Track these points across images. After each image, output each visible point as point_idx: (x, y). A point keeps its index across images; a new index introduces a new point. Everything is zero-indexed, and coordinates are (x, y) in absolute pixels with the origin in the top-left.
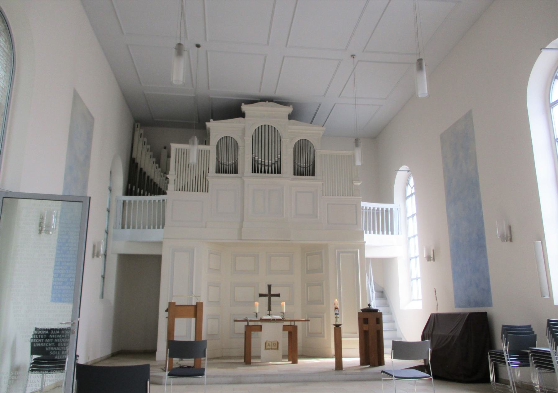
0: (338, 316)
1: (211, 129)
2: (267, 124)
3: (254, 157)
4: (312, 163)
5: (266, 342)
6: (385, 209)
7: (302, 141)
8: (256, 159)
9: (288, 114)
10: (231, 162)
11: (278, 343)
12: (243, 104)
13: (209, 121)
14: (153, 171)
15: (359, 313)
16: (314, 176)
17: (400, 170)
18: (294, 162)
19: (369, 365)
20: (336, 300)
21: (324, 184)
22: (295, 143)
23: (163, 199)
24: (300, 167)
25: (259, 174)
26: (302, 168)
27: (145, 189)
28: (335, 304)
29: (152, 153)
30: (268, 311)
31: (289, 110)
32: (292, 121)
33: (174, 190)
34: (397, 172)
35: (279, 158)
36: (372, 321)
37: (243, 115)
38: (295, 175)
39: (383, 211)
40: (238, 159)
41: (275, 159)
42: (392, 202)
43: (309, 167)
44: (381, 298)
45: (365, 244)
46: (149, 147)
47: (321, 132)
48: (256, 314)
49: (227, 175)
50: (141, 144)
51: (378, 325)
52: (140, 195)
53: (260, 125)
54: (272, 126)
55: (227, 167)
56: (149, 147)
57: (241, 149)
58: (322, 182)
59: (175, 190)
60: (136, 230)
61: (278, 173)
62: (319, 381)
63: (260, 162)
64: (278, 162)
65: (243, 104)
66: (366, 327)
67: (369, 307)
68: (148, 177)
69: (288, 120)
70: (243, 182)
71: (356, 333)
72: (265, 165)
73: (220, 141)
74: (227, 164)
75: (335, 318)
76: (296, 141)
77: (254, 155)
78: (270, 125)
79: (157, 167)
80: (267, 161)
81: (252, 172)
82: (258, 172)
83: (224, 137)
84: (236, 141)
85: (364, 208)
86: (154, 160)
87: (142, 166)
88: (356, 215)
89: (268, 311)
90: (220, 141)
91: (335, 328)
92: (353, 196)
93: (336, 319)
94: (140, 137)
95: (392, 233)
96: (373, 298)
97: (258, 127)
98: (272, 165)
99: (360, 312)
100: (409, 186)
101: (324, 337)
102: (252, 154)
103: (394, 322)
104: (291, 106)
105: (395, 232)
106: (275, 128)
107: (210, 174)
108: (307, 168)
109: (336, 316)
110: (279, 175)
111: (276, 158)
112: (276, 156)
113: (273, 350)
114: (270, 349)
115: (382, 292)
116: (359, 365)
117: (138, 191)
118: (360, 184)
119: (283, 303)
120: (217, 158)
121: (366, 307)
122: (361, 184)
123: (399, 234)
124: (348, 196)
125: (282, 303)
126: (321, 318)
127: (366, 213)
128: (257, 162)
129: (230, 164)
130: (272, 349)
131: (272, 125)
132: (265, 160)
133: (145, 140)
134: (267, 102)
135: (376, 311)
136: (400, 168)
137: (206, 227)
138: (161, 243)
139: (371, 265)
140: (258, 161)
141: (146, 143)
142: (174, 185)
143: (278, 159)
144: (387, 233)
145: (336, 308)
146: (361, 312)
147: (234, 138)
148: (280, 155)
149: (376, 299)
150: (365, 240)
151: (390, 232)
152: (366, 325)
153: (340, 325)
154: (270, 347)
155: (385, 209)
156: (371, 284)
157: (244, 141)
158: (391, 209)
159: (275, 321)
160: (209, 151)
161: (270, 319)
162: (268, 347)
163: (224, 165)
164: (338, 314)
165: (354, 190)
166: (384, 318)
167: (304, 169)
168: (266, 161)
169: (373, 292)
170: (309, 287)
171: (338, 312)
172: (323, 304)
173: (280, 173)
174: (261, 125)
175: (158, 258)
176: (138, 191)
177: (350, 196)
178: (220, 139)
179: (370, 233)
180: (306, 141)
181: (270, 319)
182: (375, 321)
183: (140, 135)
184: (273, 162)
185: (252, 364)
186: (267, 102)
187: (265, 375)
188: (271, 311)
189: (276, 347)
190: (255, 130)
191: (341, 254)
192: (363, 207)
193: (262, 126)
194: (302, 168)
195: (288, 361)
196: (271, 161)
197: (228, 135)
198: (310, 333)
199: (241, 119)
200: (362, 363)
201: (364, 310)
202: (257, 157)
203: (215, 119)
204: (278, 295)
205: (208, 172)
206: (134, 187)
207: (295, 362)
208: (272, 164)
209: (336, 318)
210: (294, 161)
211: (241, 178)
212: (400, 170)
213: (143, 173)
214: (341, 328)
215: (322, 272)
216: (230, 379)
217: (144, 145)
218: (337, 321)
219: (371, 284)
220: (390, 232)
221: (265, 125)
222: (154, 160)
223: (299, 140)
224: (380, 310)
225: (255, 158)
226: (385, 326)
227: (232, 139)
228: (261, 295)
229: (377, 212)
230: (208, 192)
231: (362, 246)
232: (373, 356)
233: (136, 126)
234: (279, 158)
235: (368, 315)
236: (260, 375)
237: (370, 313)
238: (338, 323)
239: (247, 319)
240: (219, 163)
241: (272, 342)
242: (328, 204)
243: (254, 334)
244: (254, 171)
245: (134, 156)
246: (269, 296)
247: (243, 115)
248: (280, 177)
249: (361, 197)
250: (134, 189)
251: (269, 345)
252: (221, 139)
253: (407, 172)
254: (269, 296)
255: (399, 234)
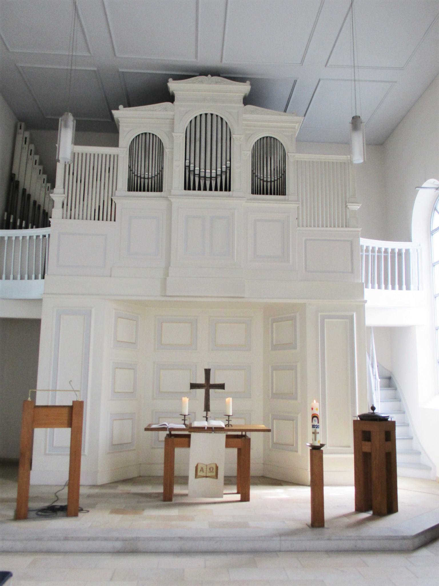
0: (318, 430)
1: (121, 121)
2: (209, 112)
3: (187, 164)
4: (282, 175)
5: (197, 465)
6: (397, 251)
7: (265, 139)
8: (192, 168)
9: (243, 95)
10: (153, 172)
11: (217, 468)
12: (170, 80)
13: (117, 109)
14: (43, 194)
15: (355, 422)
16: (284, 195)
17: (424, 188)
18: (253, 173)
19: (371, 512)
20: (315, 401)
21: (301, 207)
22: (254, 143)
23: (44, 234)
24: (262, 182)
25: (196, 192)
26: (265, 183)
27: (30, 221)
28: (312, 409)
29: (41, 168)
30: (204, 411)
31: (245, 88)
32: (249, 107)
33: (61, 217)
34: (419, 190)
35: (228, 165)
36: (378, 437)
37: (170, 98)
38: (253, 194)
39: (395, 253)
40: (162, 168)
41: (221, 168)
42: (409, 239)
43: (276, 182)
44: (388, 388)
45: (366, 304)
46: (37, 157)
47: (297, 125)
48: (185, 418)
49: (146, 193)
50: (25, 154)
51: (388, 443)
52: (21, 228)
53: (198, 114)
54: (217, 116)
55: (146, 181)
56: (37, 157)
57: (168, 153)
58: (297, 205)
59: (63, 218)
60: (11, 281)
61: (226, 190)
62: (280, 551)
63: (197, 172)
64: (226, 172)
65: (170, 80)
66: (366, 447)
67: (372, 412)
68: (35, 202)
69: (243, 105)
70: (170, 204)
71: (349, 447)
72: (205, 177)
73: (135, 139)
74: (146, 176)
75: (313, 433)
76: (256, 140)
77: (187, 161)
78: (215, 113)
79: (48, 187)
80: (209, 171)
81: (185, 189)
82: (194, 189)
83: (142, 134)
84: (161, 140)
85: (365, 248)
86: (45, 176)
87: (27, 187)
88: (352, 259)
89: (204, 411)
90: (135, 139)
91: (311, 450)
92: (346, 227)
93: (314, 435)
94: (24, 143)
95: (408, 288)
96: (375, 387)
97: (196, 118)
98: (216, 178)
99: (357, 420)
100: (435, 212)
101: (297, 451)
102: (186, 160)
103: (408, 425)
104: (248, 82)
105: (412, 286)
106: (222, 119)
107: (117, 193)
108: (273, 183)
109: (314, 431)
110: (227, 193)
111: (224, 166)
112: (224, 163)
113: (208, 479)
114: (204, 477)
115: (390, 378)
116: (353, 508)
117: (18, 224)
118: (359, 207)
119: (229, 400)
120: (129, 167)
121: (367, 411)
122: (360, 208)
123: (418, 290)
124: (338, 227)
125: (227, 400)
126: (293, 420)
127: (367, 257)
128: (193, 172)
129: (150, 177)
130: (206, 477)
131: (217, 114)
132: (205, 170)
133: (32, 147)
134: (209, 76)
135: (384, 419)
136: (423, 183)
137: (111, 276)
138: (39, 301)
139: (373, 339)
140: (194, 171)
141: (33, 152)
142: (61, 210)
143: (226, 167)
144: (393, 288)
145: (314, 416)
146: (359, 419)
147: (158, 135)
148: (230, 161)
149: (380, 390)
150: (366, 298)
151: (404, 286)
152: (367, 443)
153: (322, 445)
154: (204, 474)
155: (397, 251)
156: (373, 367)
157: (172, 139)
158: (407, 251)
159: (213, 431)
160: (118, 156)
161: (205, 428)
162: (199, 474)
163: (141, 178)
164: (317, 427)
165: (348, 217)
166: (398, 431)
167: (269, 184)
168: (208, 171)
169: (375, 378)
170: (274, 372)
171: (318, 423)
172: (296, 399)
173: (230, 190)
174: (200, 114)
175: (36, 324)
176: (18, 224)
177: (342, 227)
178: (134, 136)
179: (373, 287)
180: (272, 139)
181: (205, 428)
182: (383, 436)
183: (24, 139)
184: (219, 173)
185: (175, 500)
186: (209, 76)
187: (181, 538)
188: (209, 412)
189: (214, 474)
190: (191, 122)
191: (326, 320)
192: (362, 246)
193: (201, 115)
194: (265, 183)
195: (236, 491)
196: (215, 171)
197: (148, 131)
198: (274, 443)
199: (168, 104)
200: (359, 509)
201: (364, 418)
202: (192, 165)
203: (129, 104)
204: (222, 386)
205: (116, 189)
206: (12, 216)
207: (245, 498)
208: (217, 175)
209: (315, 433)
210: (252, 171)
211: (166, 198)
212: (424, 188)
213: (27, 196)
214: (322, 451)
215: (296, 348)
216: (118, 545)
217: (31, 154)
218: (315, 440)
219: (373, 367)
220: (404, 286)
221: (206, 114)
222: (45, 176)
223: (260, 139)
224: (393, 417)
225: (189, 166)
226: (400, 445)
227: (155, 137)
228: (194, 386)
229: (384, 256)
230: (115, 221)
231: (360, 309)
232: (379, 498)
233: (19, 127)
234: (228, 165)
235: (368, 426)
236: (172, 539)
237: (376, 422)
238: (317, 444)
239: (165, 426)
240: (133, 175)
241: (206, 465)
242: (306, 240)
243: (179, 452)
244: (188, 186)
245: (15, 171)
246: (206, 388)
247: (170, 98)
248: (229, 196)
249: (360, 229)
250: (11, 221)
251: (202, 470)
252: (136, 137)
253: (434, 190)
254: (206, 388)
255: (418, 290)
